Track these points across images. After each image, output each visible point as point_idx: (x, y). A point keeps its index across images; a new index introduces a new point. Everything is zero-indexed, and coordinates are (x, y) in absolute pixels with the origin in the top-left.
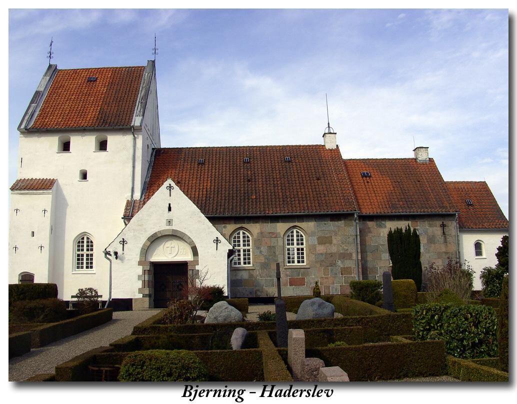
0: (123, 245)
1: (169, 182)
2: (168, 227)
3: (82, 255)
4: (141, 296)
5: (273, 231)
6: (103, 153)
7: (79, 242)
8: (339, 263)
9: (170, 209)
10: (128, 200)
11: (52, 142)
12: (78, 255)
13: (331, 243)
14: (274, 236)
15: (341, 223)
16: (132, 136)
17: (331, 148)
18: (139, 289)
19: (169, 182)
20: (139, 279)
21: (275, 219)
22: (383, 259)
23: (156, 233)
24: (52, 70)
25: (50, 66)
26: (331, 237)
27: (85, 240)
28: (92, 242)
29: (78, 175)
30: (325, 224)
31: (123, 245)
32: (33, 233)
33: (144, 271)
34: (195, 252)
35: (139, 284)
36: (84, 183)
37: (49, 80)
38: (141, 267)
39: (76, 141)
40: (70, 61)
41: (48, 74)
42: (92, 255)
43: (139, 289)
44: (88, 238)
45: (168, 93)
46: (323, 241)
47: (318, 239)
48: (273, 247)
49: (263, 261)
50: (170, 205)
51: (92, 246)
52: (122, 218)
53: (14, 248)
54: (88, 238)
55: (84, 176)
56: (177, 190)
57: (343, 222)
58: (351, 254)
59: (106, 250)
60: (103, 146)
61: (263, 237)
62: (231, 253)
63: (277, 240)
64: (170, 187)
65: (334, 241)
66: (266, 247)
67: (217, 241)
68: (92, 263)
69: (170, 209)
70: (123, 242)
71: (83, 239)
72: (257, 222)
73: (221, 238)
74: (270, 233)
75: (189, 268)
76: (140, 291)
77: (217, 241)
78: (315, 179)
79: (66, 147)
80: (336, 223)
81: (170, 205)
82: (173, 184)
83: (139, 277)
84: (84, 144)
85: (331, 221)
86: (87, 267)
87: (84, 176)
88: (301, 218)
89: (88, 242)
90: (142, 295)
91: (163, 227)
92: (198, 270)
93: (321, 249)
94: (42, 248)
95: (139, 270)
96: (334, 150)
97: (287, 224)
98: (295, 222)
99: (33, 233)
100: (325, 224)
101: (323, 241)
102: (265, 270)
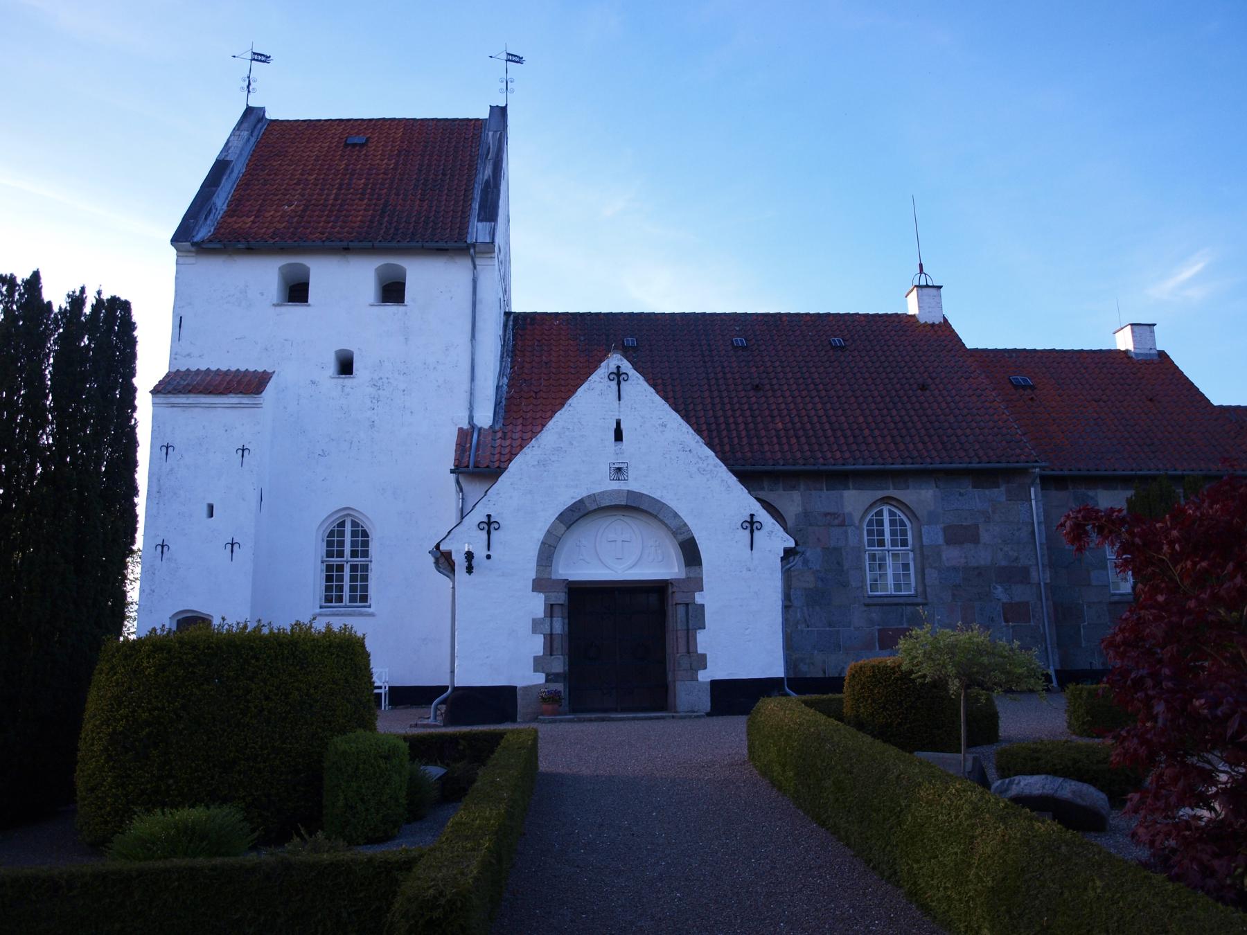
0: (489, 533)
1: (615, 360)
2: (615, 485)
3: (340, 568)
4: (540, 679)
5: (832, 511)
6: (391, 309)
7: (331, 534)
8: (999, 591)
9: (618, 436)
10: (461, 430)
11: (264, 274)
12: (329, 568)
13: (975, 540)
14: (836, 522)
15: (999, 493)
16: (469, 263)
17: (930, 322)
18: (536, 659)
19: (615, 360)
20: (534, 631)
21: (840, 478)
22: (1094, 583)
23: (581, 501)
24: (252, 115)
25: (249, 111)
26: (977, 527)
27: (348, 529)
28: (365, 534)
29: (332, 366)
30: (961, 494)
31: (489, 533)
32: (211, 507)
33: (550, 609)
34: (690, 552)
35: (537, 645)
36: (347, 381)
37: (248, 140)
38: (542, 596)
39: (325, 274)
40: (489, 262)
41: (245, 125)
42: (365, 568)
43: (536, 659)
44: (355, 524)
45: (532, 185)
46: (959, 535)
47: (945, 530)
48: (835, 549)
49: (811, 586)
50: (618, 423)
51: (366, 544)
52: (452, 471)
53: (159, 548)
54: (355, 524)
55: (346, 366)
56: (638, 388)
57: (1003, 489)
58: (1025, 571)
59: (438, 546)
60: (392, 291)
61: (811, 525)
62: (788, 553)
63: (846, 532)
64: (618, 376)
65: (985, 537)
66: (819, 549)
67: (752, 524)
68: (365, 588)
69: (618, 436)
70: (489, 523)
71: (342, 524)
72: (793, 488)
73: (763, 515)
74: (826, 514)
75: (678, 598)
76: (538, 664)
77: (752, 524)
78: (915, 386)
79: (297, 292)
80: (987, 492)
81: (618, 423)
82: (626, 366)
83: (536, 625)
84: (343, 282)
85: (974, 487)
86: (353, 599)
87: (346, 366)
88: (902, 477)
89: (354, 534)
90: (543, 675)
91: (601, 483)
92: (703, 606)
93: (952, 556)
94: (236, 547)
95: (537, 605)
96: (940, 325)
97: (870, 492)
98: (888, 489)
99: (211, 507)
100: (961, 494)
101: (959, 535)
102: (817, 608)
